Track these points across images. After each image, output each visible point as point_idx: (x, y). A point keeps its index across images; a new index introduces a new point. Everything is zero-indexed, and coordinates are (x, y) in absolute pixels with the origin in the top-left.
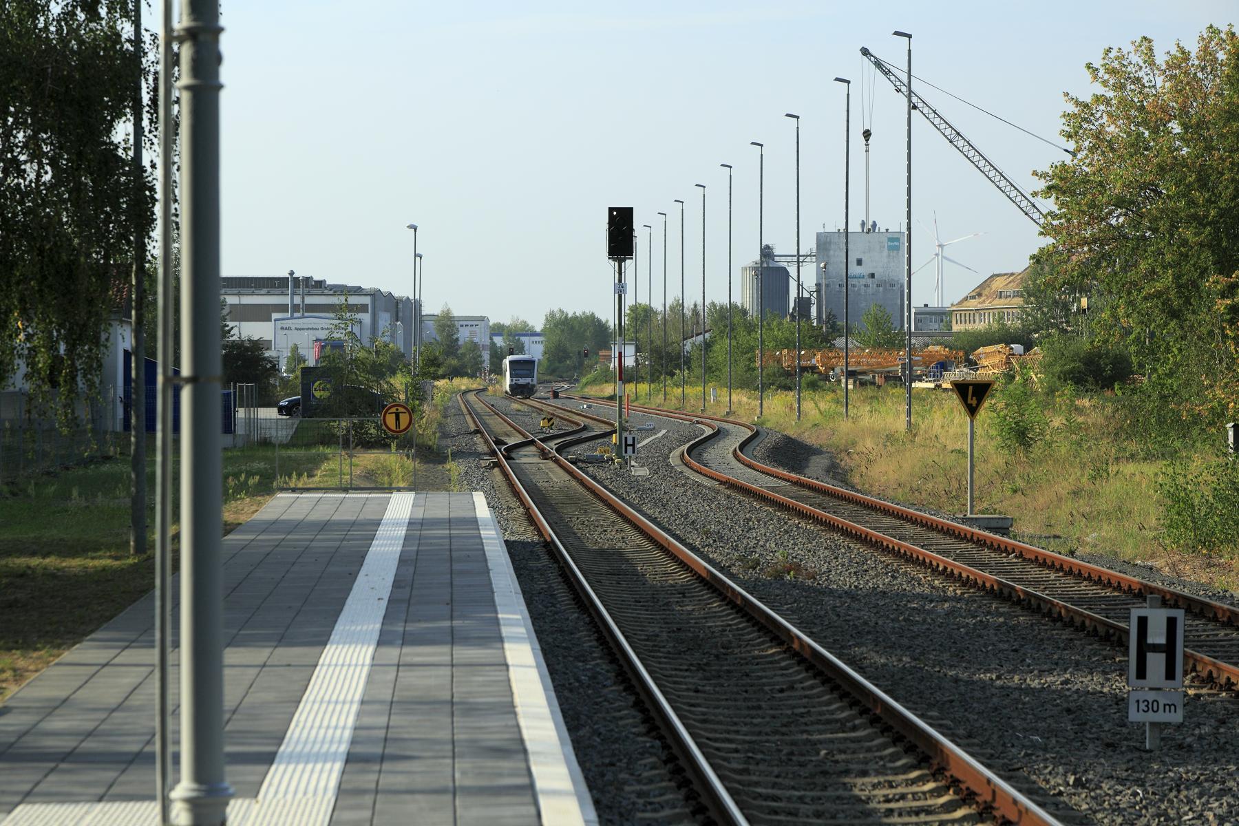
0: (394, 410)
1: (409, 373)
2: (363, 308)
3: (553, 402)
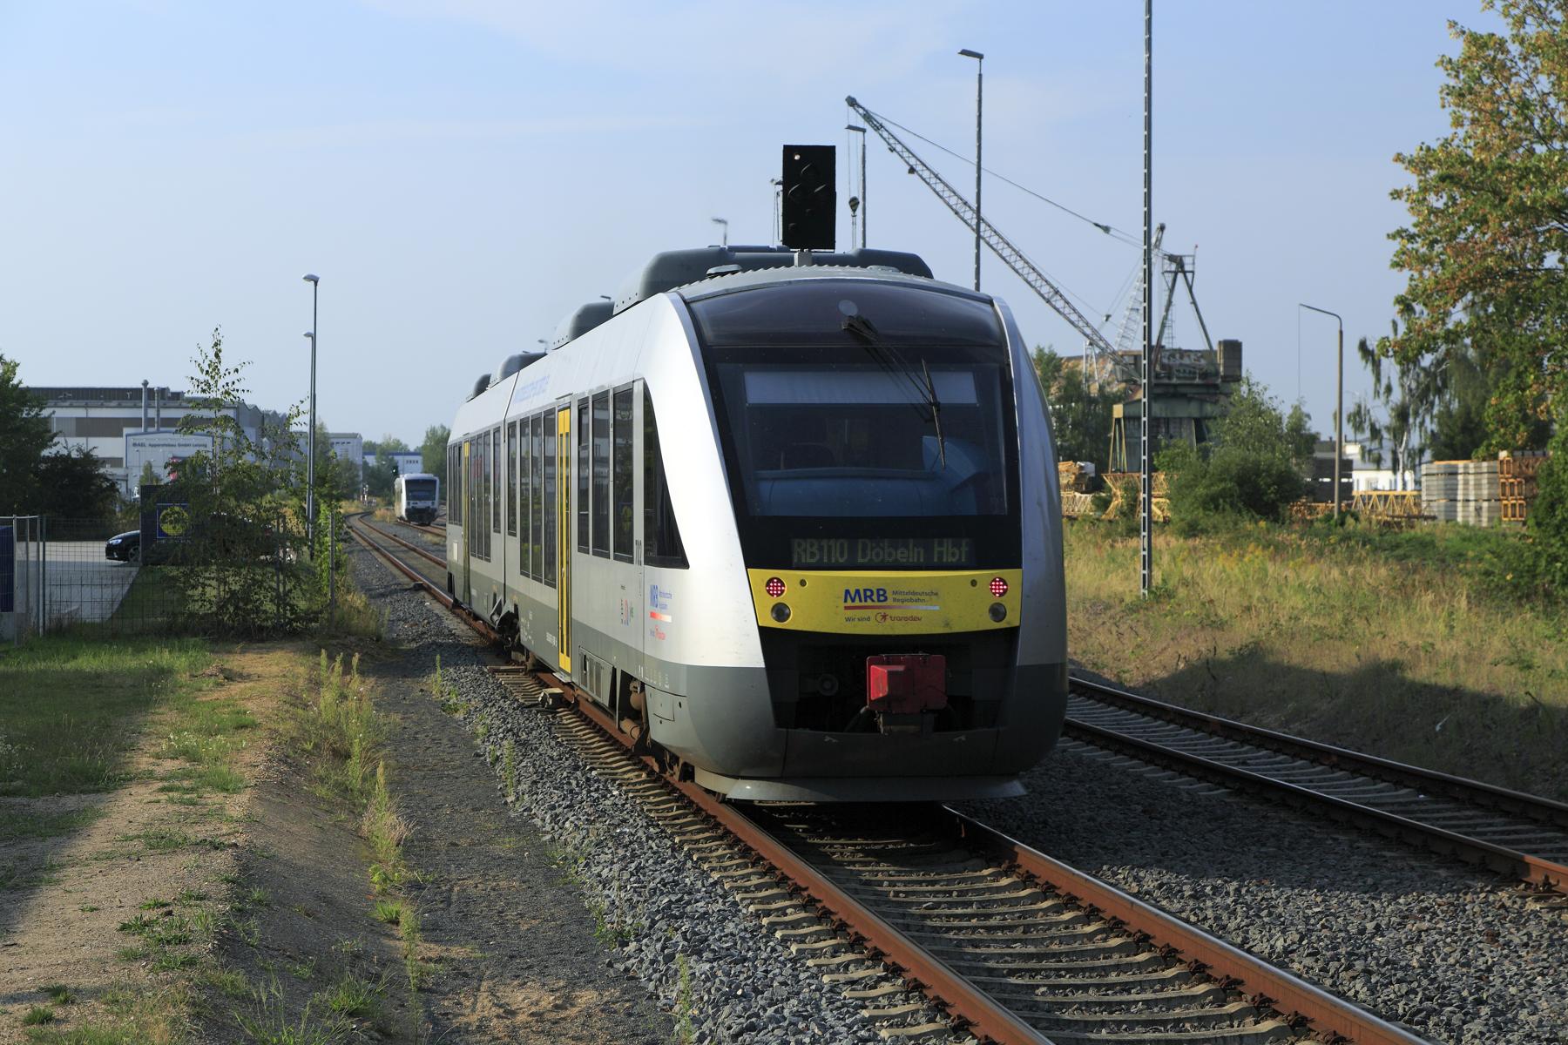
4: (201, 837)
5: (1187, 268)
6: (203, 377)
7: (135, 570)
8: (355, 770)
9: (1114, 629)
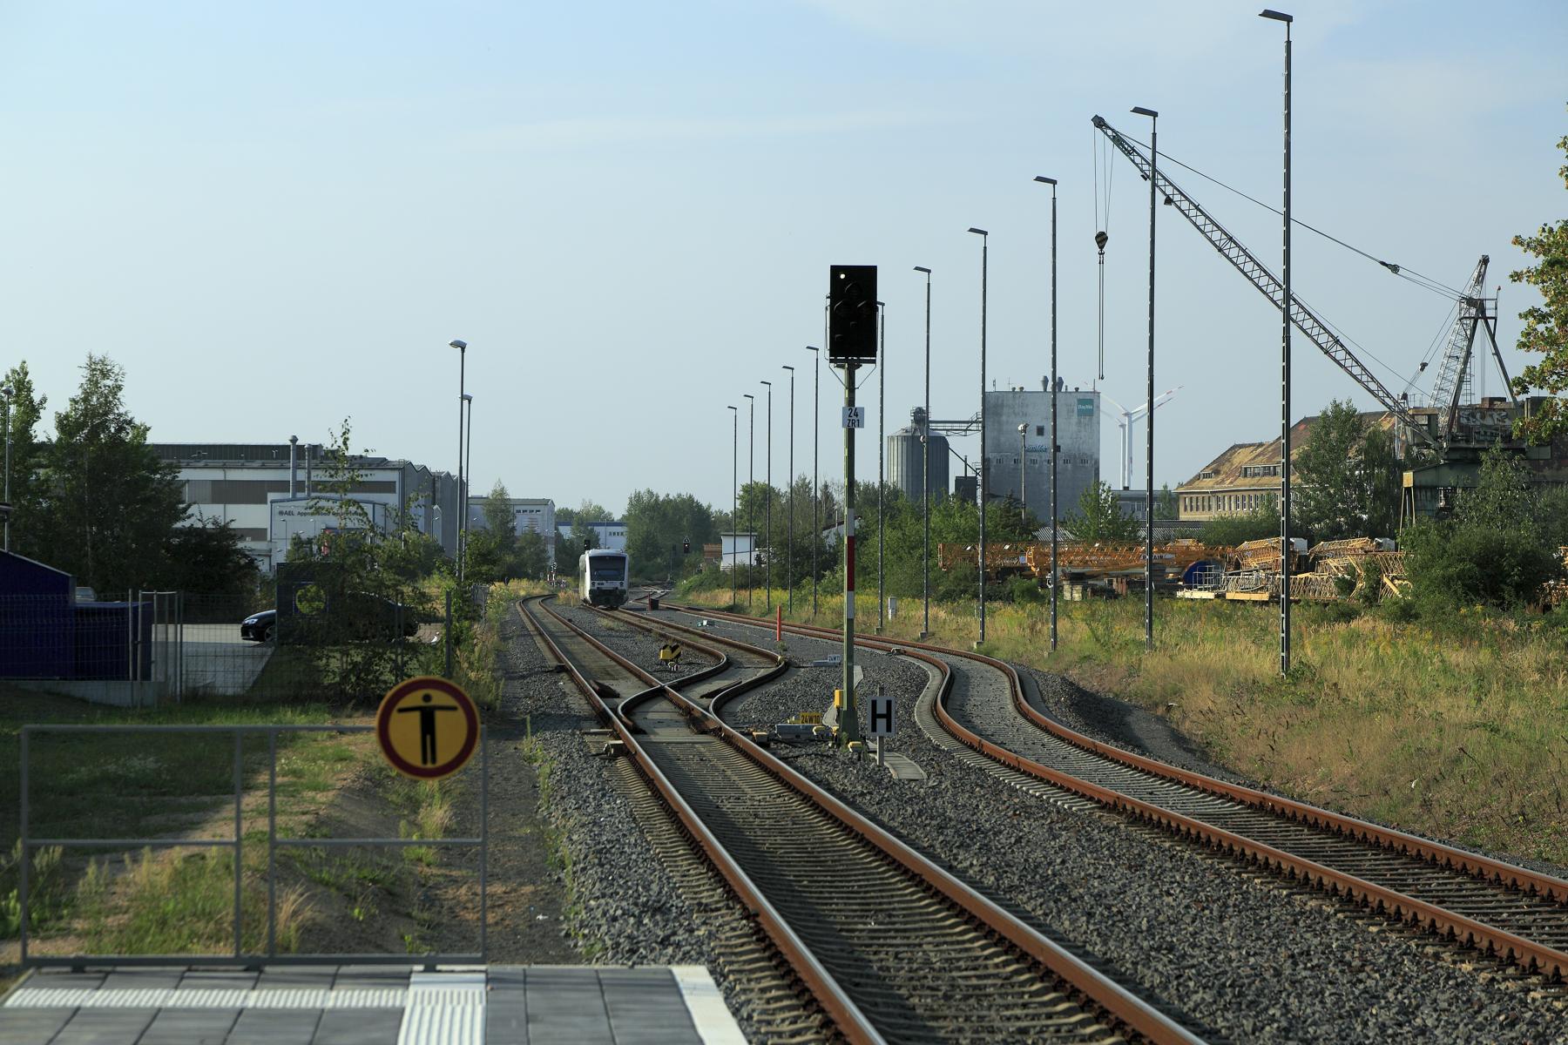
0: (415, 699)
1: (452, 573)
2: (387, 487)
3: (650, 614)
5: (1489, 314)
7: (270, 651)
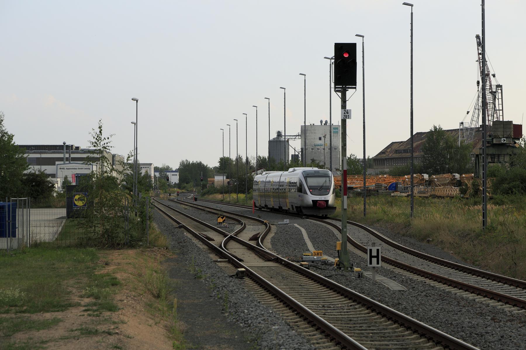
4: (103, 330)
6: (94, 140)
8: (485, 329)
9: (472, 243)
